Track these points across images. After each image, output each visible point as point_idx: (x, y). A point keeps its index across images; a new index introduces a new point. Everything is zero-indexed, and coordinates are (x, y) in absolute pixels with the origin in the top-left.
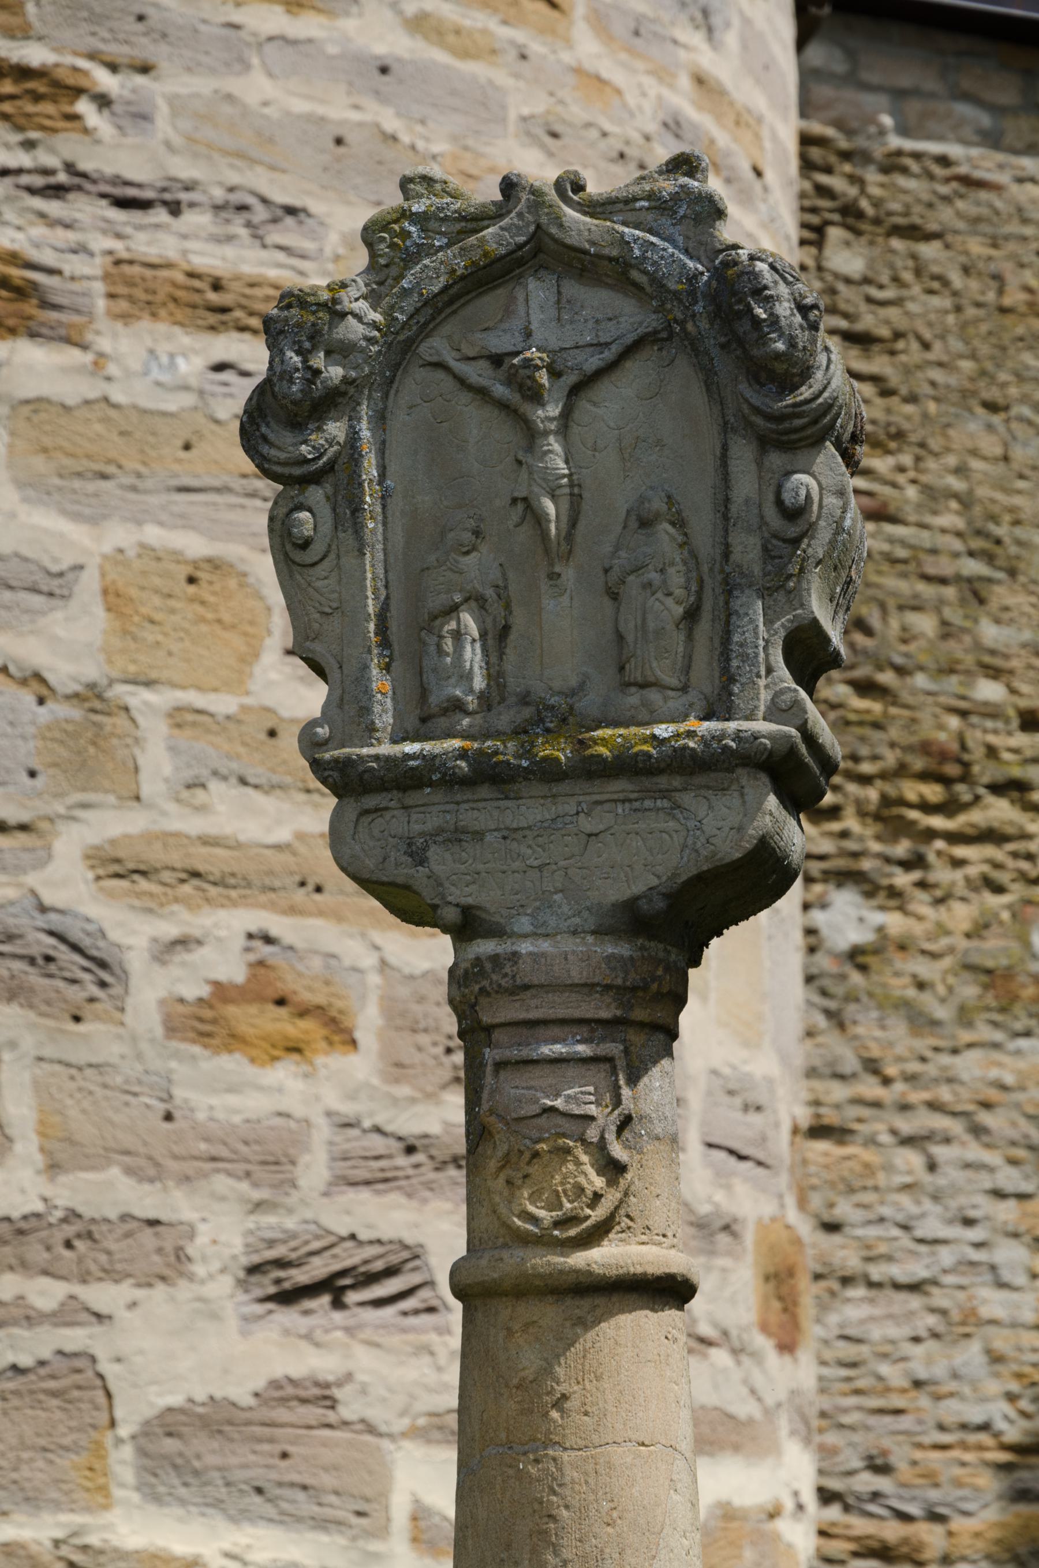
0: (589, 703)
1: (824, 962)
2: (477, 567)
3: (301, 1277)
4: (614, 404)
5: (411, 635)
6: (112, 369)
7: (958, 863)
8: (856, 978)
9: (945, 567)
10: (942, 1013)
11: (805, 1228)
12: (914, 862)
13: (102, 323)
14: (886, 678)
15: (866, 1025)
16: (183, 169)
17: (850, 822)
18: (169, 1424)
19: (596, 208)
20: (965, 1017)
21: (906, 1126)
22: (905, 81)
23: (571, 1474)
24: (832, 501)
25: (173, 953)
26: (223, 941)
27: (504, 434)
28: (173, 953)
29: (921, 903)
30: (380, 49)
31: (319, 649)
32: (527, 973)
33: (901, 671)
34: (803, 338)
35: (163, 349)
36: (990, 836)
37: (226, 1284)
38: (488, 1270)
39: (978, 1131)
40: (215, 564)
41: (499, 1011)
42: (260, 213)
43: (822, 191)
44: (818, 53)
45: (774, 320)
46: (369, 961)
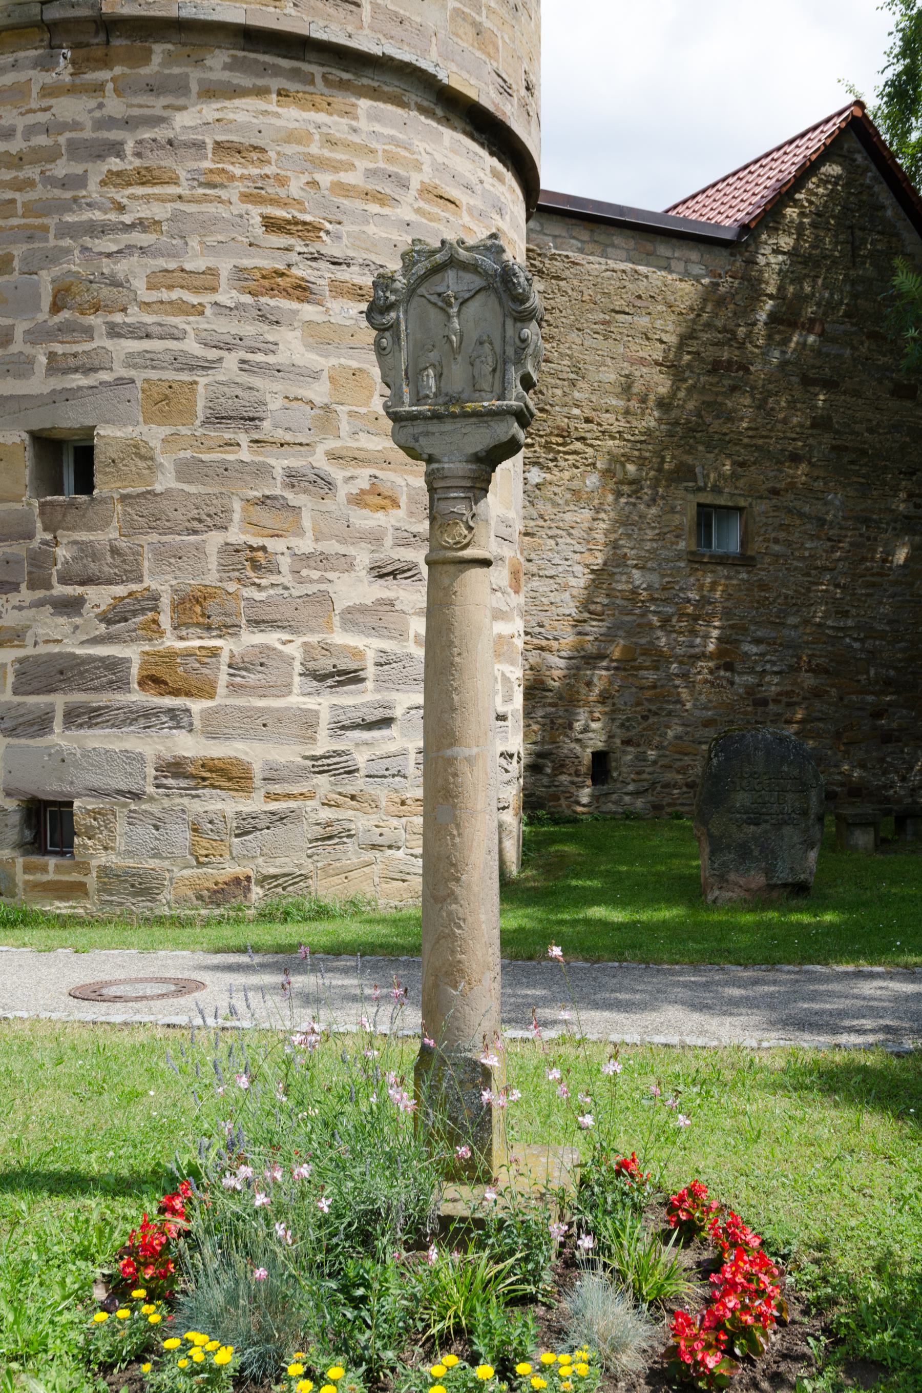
0: (465, 396)
1: (528, 487)
2: (434, 356)
3: (385, 571)
4: (473, 308)
5: (414, 376)
6: (331, 312)
7: (566, 460)
8: (537, 492)
9: (565, 376)
10: (560, 502)
11: (522, 560)
12: (554, 460)
13: (328, 299)
14: (548, 407)
15: (540, 505)
16: (351, 253)
17: (537, 448)
18: (349, 610)
19: (468, 249)
20: (567, 503)
21: (550, 533)
22: (557, 233)
23: (458, 613)
24: (535, 337)
25: (350, 481)
26: (363, 477)
27: (441, 316)
28: (350, 481)
29: (556, 471)
30: (407, 218)
31: (388, 380)
32: (446, 473)
33: (551, 405)
34: (527, 288)
35: (345, 307)
36: (575, 452)
37: (365, 572)
38: (435, 556)
39: (570, 534)
40: (360, 370)
41: (439, 484)
42: (373, 267)
43: (532, 265)
44: (532, 224)
45: (519, 283)
46: (404, 483)
